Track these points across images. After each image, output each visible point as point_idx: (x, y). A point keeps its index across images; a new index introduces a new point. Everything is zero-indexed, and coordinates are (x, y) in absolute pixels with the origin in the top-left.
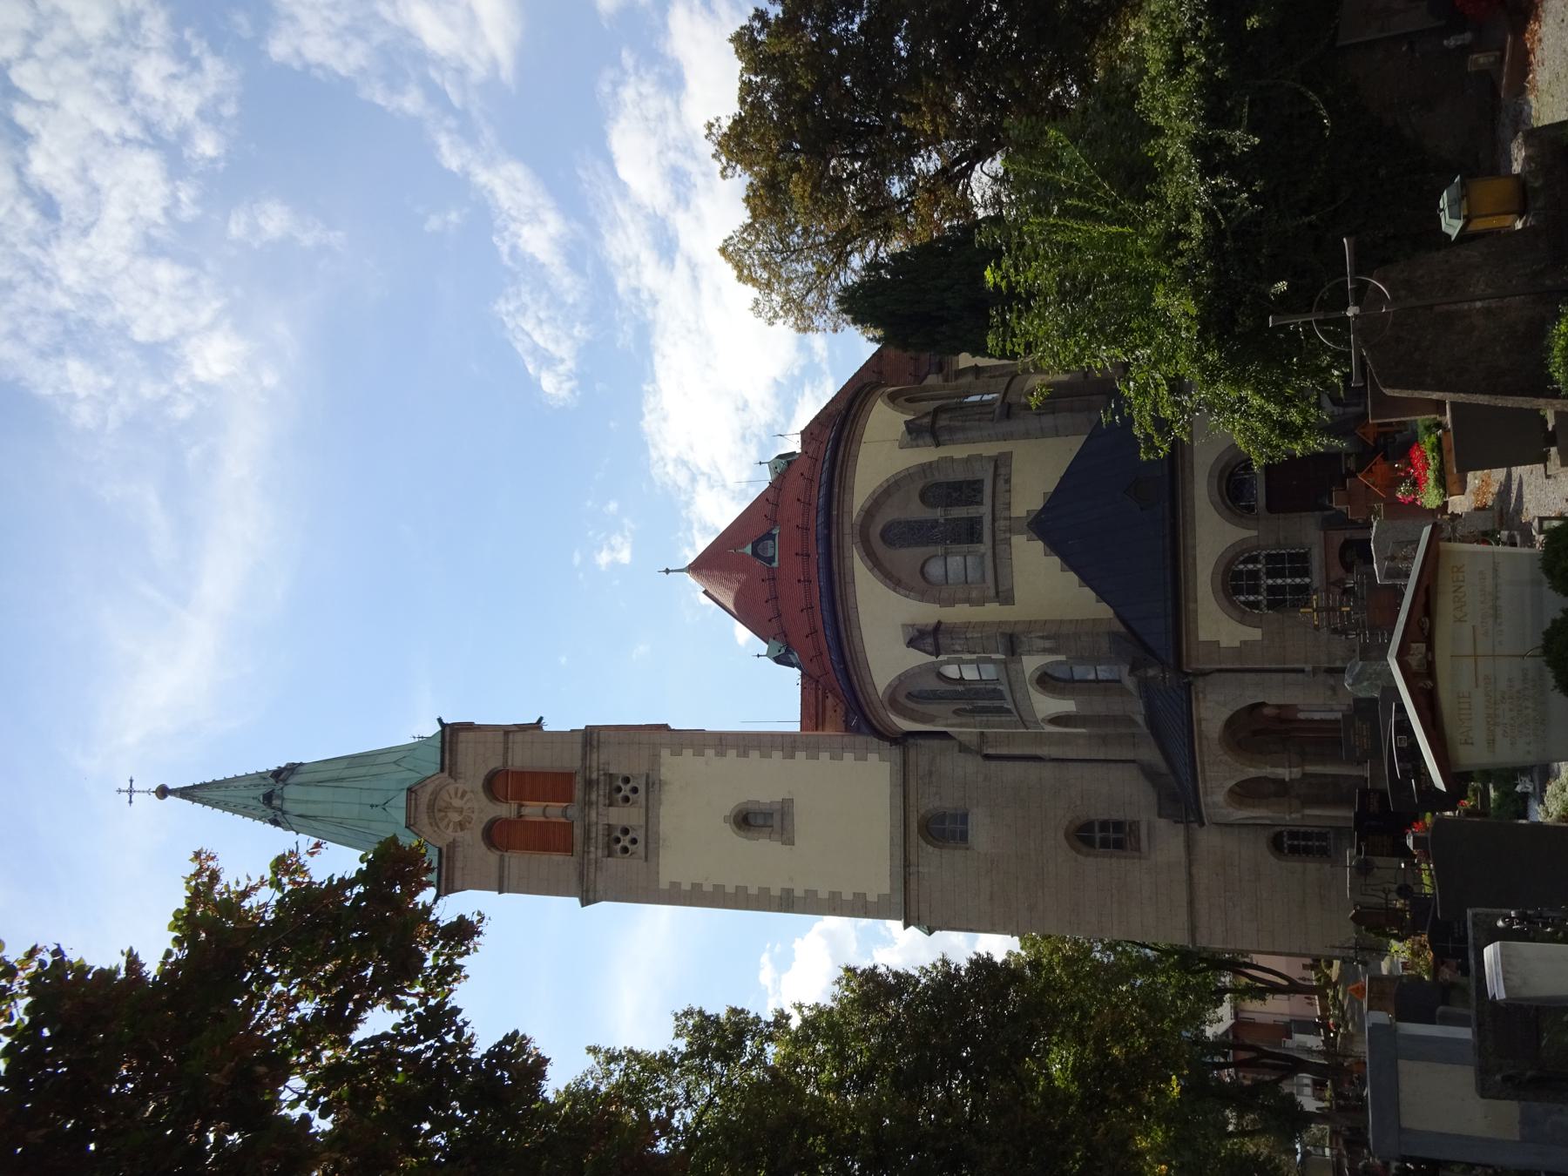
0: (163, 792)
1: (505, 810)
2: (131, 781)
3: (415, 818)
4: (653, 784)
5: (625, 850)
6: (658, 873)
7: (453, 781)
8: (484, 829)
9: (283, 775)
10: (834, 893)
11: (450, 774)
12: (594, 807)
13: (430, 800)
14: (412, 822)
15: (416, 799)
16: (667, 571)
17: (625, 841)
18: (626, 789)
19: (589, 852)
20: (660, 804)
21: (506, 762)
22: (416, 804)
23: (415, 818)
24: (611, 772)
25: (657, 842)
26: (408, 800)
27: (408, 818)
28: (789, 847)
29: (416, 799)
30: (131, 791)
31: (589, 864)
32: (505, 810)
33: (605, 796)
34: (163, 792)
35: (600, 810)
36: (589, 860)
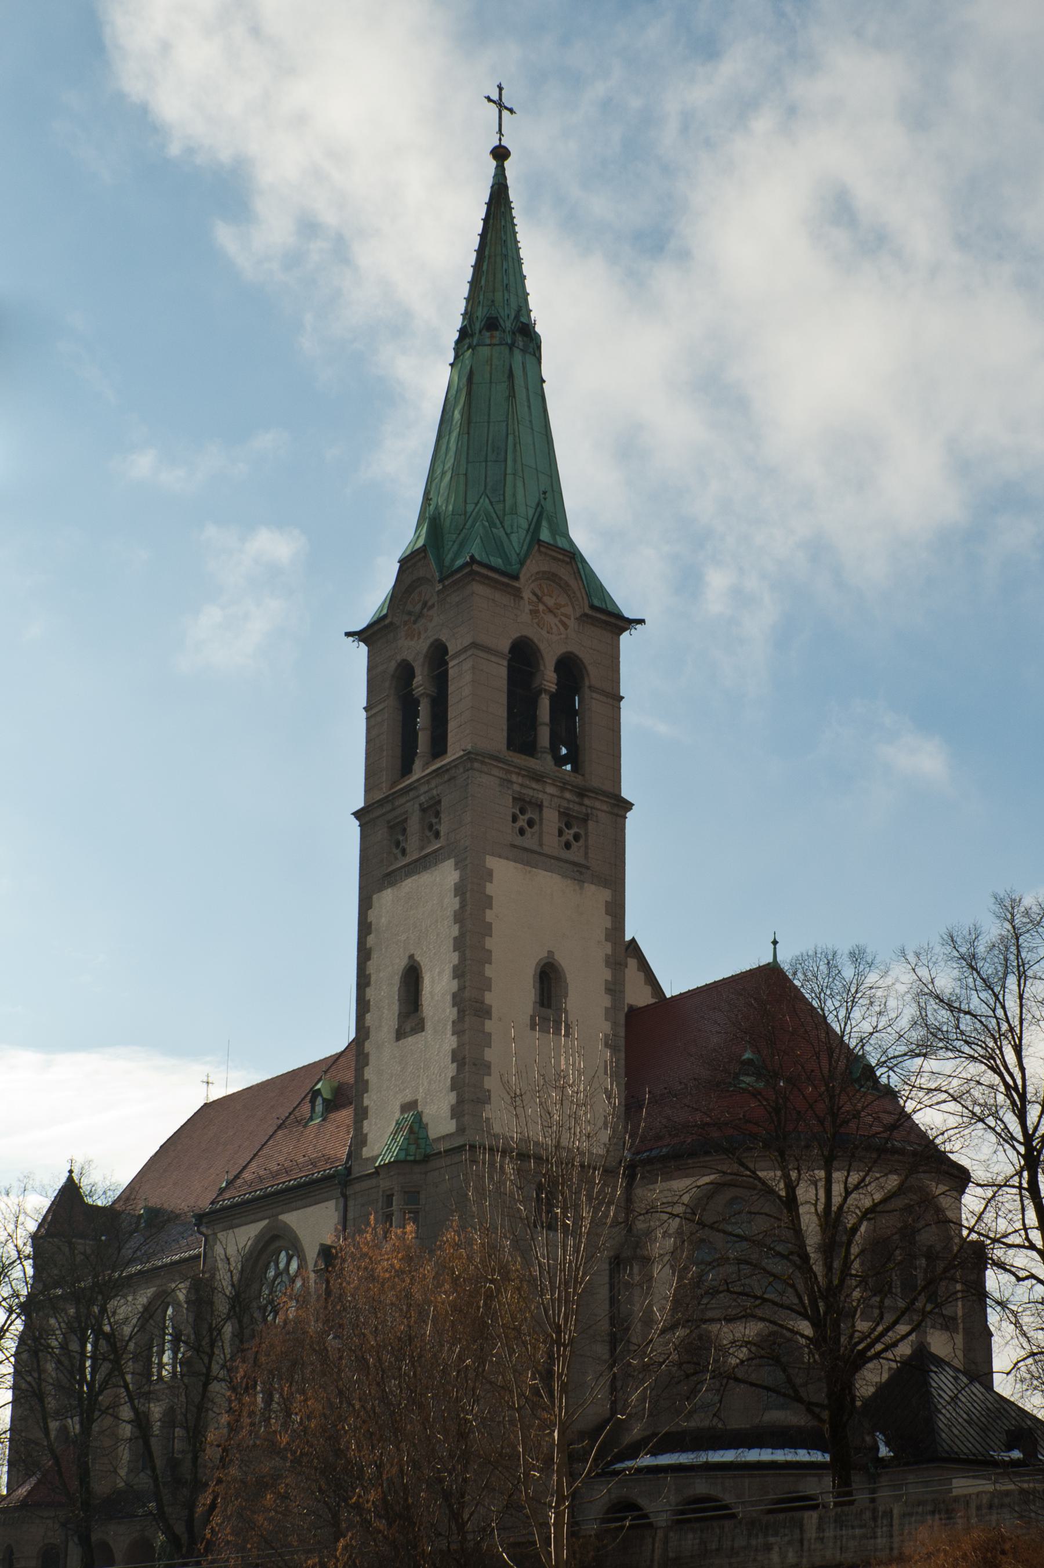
3: (546, 554)
4: (581, 873)
6: (500, 857)
7: (578, 615)
8: (531, 640)
10: (489, 1067)
11: (586, 615)
12: (577, 800)
13: (561, 579)
14: (542, 549)
15: (563, 561)
16: (775, 943)
19: (519, 774)
20: (563, 876)
22: (559, 560)
23: (546, 554)
24: (590, 822)
25: (528, 863)
28: (529, 1023)
29: (563, 561)
31: (508, 772)
33: (568, 809)
34: (500, 154)
35: (556, 800)
36: (511, 772)
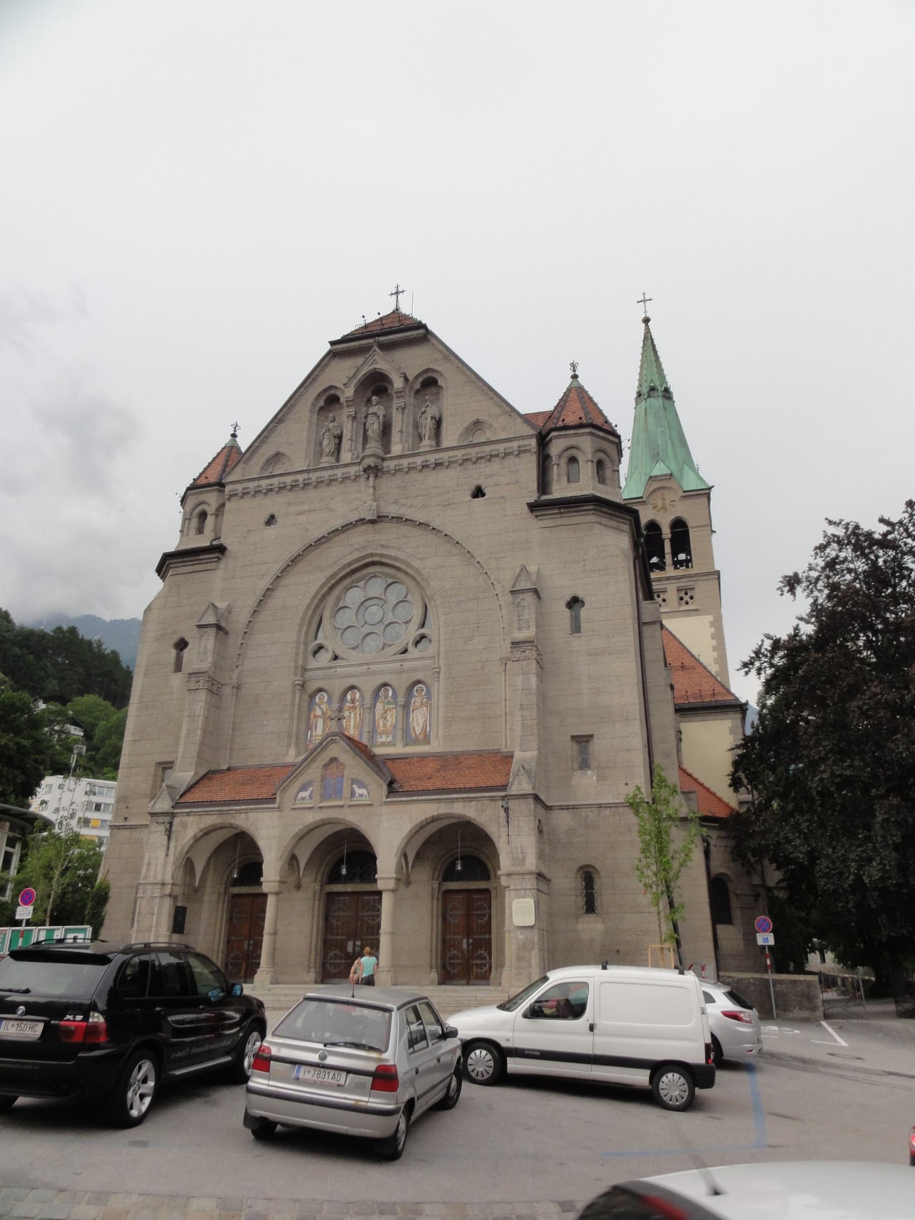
0: (646, 321)
1: (666, 532)
2: (650, 300)
5: (681, 599)
9: (667, 394)
11: (683, 497)
17: (686, 598)
18: (686, 598)
21: (693, 527)
26: (666, 475)
27: (656, 476)
30: (644, 301)
32: (666, 532)
